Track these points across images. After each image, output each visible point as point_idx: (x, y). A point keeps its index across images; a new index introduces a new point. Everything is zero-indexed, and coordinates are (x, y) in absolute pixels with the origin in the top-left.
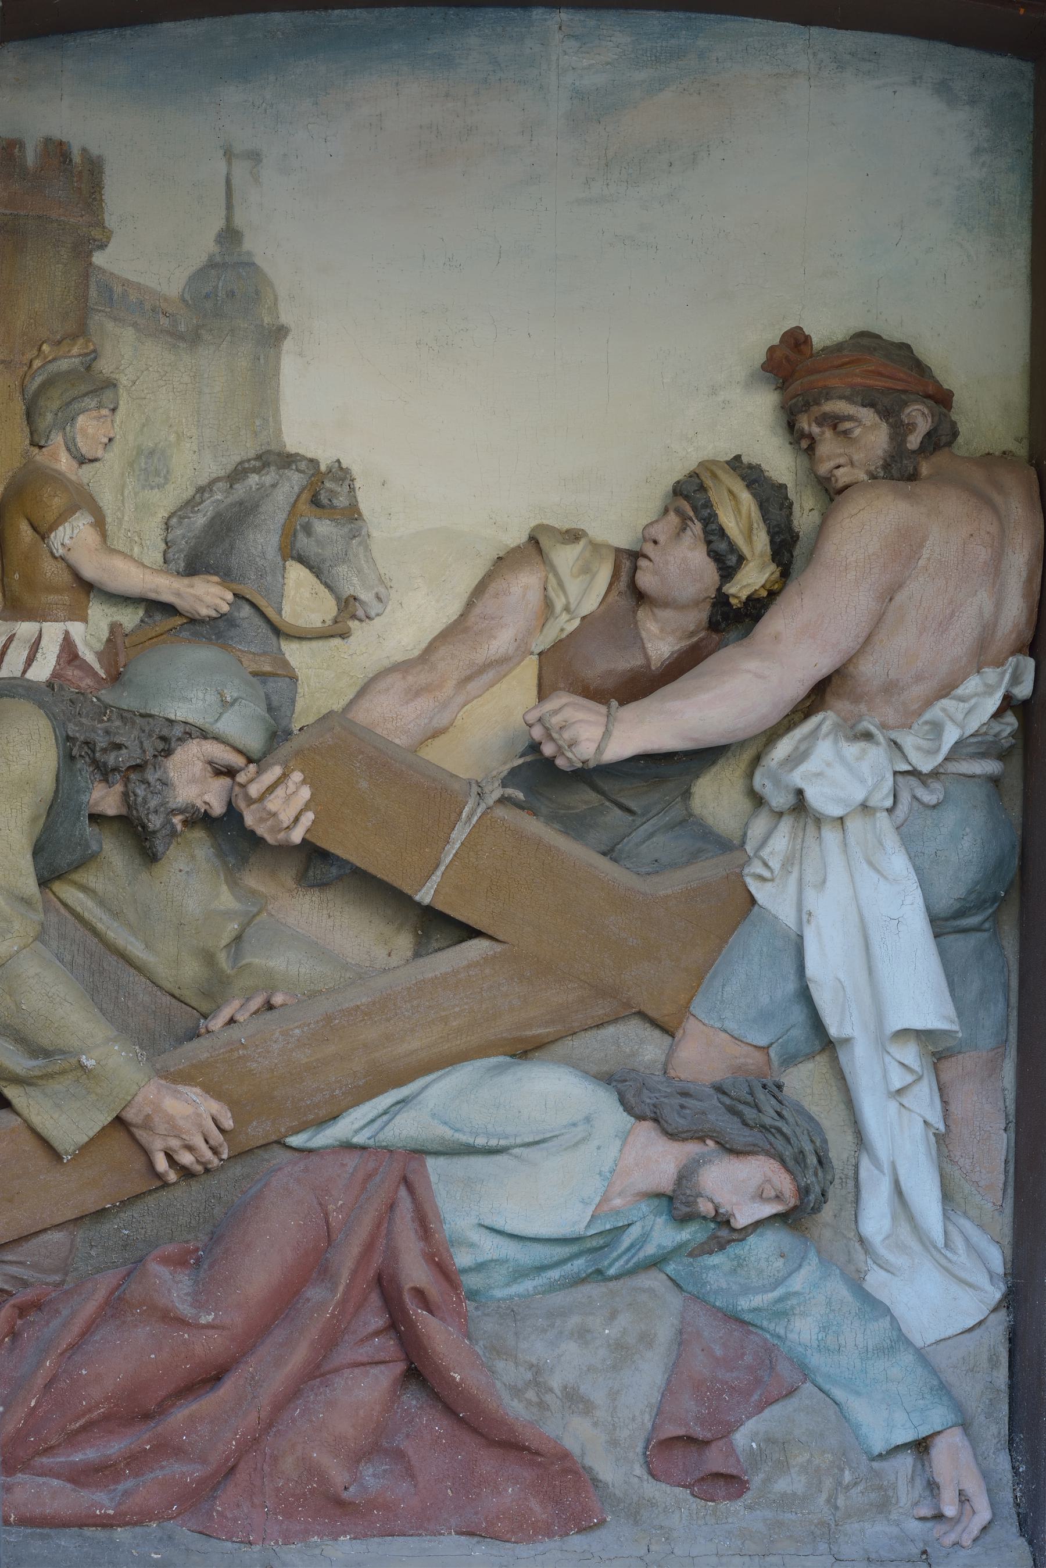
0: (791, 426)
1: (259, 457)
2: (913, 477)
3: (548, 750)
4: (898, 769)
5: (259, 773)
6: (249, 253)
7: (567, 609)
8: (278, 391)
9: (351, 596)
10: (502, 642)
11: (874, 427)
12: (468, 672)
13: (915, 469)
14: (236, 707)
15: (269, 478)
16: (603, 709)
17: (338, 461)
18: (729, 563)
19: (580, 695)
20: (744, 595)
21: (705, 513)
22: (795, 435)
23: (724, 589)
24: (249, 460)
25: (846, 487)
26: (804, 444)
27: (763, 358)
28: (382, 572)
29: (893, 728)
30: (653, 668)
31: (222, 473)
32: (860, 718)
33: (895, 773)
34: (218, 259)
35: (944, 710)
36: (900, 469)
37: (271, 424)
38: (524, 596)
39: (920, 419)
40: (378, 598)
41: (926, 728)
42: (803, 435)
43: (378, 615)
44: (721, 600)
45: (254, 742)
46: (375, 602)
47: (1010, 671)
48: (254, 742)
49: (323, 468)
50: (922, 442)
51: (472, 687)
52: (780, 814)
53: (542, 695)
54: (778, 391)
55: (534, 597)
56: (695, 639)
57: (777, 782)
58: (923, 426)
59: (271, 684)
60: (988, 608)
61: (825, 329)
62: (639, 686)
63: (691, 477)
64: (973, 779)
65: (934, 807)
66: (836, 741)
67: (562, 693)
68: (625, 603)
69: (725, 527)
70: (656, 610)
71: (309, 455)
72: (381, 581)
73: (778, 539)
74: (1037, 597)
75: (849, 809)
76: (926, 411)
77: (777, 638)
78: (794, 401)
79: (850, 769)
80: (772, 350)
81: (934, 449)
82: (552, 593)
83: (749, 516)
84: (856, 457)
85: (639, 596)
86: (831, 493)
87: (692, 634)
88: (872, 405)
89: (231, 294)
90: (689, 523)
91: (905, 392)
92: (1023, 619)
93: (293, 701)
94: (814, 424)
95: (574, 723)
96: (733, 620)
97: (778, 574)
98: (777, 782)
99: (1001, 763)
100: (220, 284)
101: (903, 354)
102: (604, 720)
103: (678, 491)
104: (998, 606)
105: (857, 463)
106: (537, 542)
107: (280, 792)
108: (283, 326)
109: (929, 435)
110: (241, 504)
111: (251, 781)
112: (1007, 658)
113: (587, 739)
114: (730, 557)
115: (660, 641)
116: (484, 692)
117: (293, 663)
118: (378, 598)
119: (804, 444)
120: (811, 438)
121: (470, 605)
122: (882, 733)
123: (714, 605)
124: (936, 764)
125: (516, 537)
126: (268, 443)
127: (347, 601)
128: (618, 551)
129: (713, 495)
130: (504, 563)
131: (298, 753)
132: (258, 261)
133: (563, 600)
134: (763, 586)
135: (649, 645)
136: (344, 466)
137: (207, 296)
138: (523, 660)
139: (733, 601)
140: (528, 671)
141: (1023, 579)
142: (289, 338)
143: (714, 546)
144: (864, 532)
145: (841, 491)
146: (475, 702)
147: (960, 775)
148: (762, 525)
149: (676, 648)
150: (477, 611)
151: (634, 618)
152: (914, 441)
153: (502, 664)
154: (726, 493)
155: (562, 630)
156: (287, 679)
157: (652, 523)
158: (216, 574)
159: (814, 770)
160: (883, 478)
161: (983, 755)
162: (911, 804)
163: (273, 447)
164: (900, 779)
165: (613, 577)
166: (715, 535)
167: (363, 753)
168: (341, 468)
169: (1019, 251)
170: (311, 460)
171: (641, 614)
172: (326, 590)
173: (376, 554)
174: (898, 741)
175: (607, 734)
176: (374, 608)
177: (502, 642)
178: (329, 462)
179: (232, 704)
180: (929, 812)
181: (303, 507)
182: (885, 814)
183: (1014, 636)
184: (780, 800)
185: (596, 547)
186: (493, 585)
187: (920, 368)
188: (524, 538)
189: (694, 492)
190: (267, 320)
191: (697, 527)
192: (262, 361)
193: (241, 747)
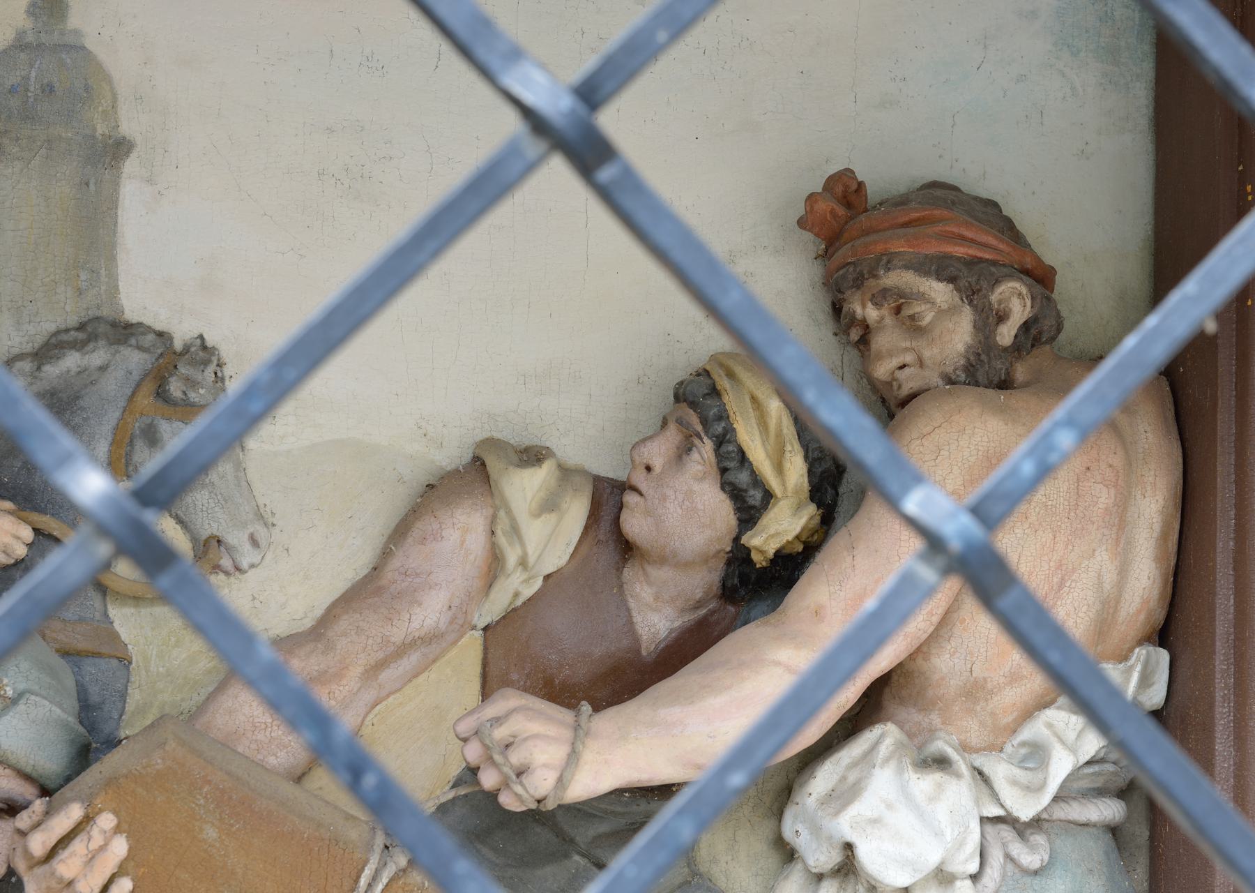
0: (837, 309)
1: (81, 327)
2: (1005, 384)
3: (488, 780)
4: (986, 814)
5: (48, 813)
6: (77, 33)
7: (523, 563)
8: (115, 232)
9: (212, 537)
10: (429, 612)
11: (952, 310)
12: (381, 655)
13: (1008, 373)
14: (21, 707)
15: (98, 357)
16: (566, 715)
17: (201, 337)
18: (751, 502)
19: (535, 694)
20: (771, 550)
21: (719, 428)
22: (844, 321)
23: (744, 540)
24: (67, 331)
25: (913, 396)
26: (857, 338)
27: (800, 210)
28: (261, 501)
29: (977, 751)
30: (644, 653)
31: (28, 348)
32: (932, 733)
33: (984, 820)
34: (30, 38)
35: (1049, 726)
36: (990, 374)
37: (104, 279)
38: (462, 543)
39: (1015, 300)
40: (254, 542)
41: (1023, 751)
42: (853, 321)
43: (252, 566)
44: (739, 557)
45: (50, 761)
46: (247, 546)
47: (1138, 668)
48: (50, 761)
49: (178, 345)
50: (1016, 336)
51: (388, 676)
52: (820, 877)
53: (486, 692)
54: (819, 261)
55: (477, 543)
56: (703, 612)
57: (816, 830)
58: (1019, 311)
59: (89, 667)
60: (1110, 578)
61: (883, 174)
62: (626, 678)
63: (699, 375)
64: (1087, 829)
65: (1035, 873)
66: (900, 771)
67: (509, 691)
68: (606, 556)
69: (745, 449)
70: (649, 569)
71: (158, 327)
72: (259, 516)
73: (819, 470)
74: (1173, 563)
75: (918, 876)
76: (1024, 290)
77: (818, 613)
78: (841, 272)
79: (920, 814)
80: (811, 198)
81: (1033, 346)
82: (502, 540)
83: (779, 434)
84: (927, 354)
85: (626, 549)
86: (891, 406)
87: (699, 604)
88: (952, 280)
89: (49, 89)
90: (697, 441)
91: (994, 263)
92: (1155, 593)
93: (123, 696)
94: (869, 305)
95: (526, 739)
96: (755, 585)
97: (817, 519)
98: (816, 830)
99: (1123, 804)
100: (33, 74)
101: (990, 213)
102: (567, 734)
103: (681, 395)
104: (1123, 572)
105: (928, 362)
106: (483, 464)
107: (78, 846)
108: (124, 138)
109: (1026, 326)
110: (52, 395)
111: (36, 826)
112: (1131, 650)
113: (545, 766)
114: (752, 492)
115: (655, 618)
116: (405, 684)
117: (124, 636)
118: (254, 542)
119: (855, 335)
120: (866, 329)
121: (386, 554)
122: (964, 759)
123: (729, 563)
124: (1040, 808)
125: (451, 455)
126: (98, 307)
127: (206, 543)
128: (598, 481)
129: (731, 401)
130: (437, 492)
131: (111, 782)
132: (90, 44)
133: (519, 551)
134: (798, 537)
135: (637, 618)
136: (209, 343)
137: (13, 90)
138: (462, 637)
139: (755, 557)
140: (469, 650)
141: (1155, 535)
142: (133, 155)
143: (730, 477)
144: (941, 472)
145: (904, 403)
146: (391, 699)
147: (1070, 822)
148: (797, 446)
149: (677, 624)
150: (395, 563)
151: (619, 578)
152: (1006, 334)
153: (431, 643)
154: (748, 400)
155: (516, 595)
156: (115, 662)
157: (644, 441)
158: (11, 499)
159: (869, 814)
160: (965, 383)
161: (1100, 792)
162: (1004, 868)
163: (105, 312)
164: (989, 828)
165: (589, 517)
166: (733, 459)
167: (209, 782)
168: (204, 347)
169: (1138, 84)
170: (160, 334)
171: (628, 573)
172: (178, 527)
173: (253, 473)
174: (986, 770)
175: (573, 757)
176: (247, 556)
177: (429, 612)
178: (187, 337)
179: (14, 701)
180: (1028, 880)
181: (146, 400)
182: (968, 882)
183: (1142, 617)
184: (820, 857)
185: (566, 473)
186: (419, 525)
187: (1009, 229)
188: (467, 458)
189: (704, 396)
190: (101, 129)
191: (706, 448)
192: (92, 187)
193: (29, 770)
